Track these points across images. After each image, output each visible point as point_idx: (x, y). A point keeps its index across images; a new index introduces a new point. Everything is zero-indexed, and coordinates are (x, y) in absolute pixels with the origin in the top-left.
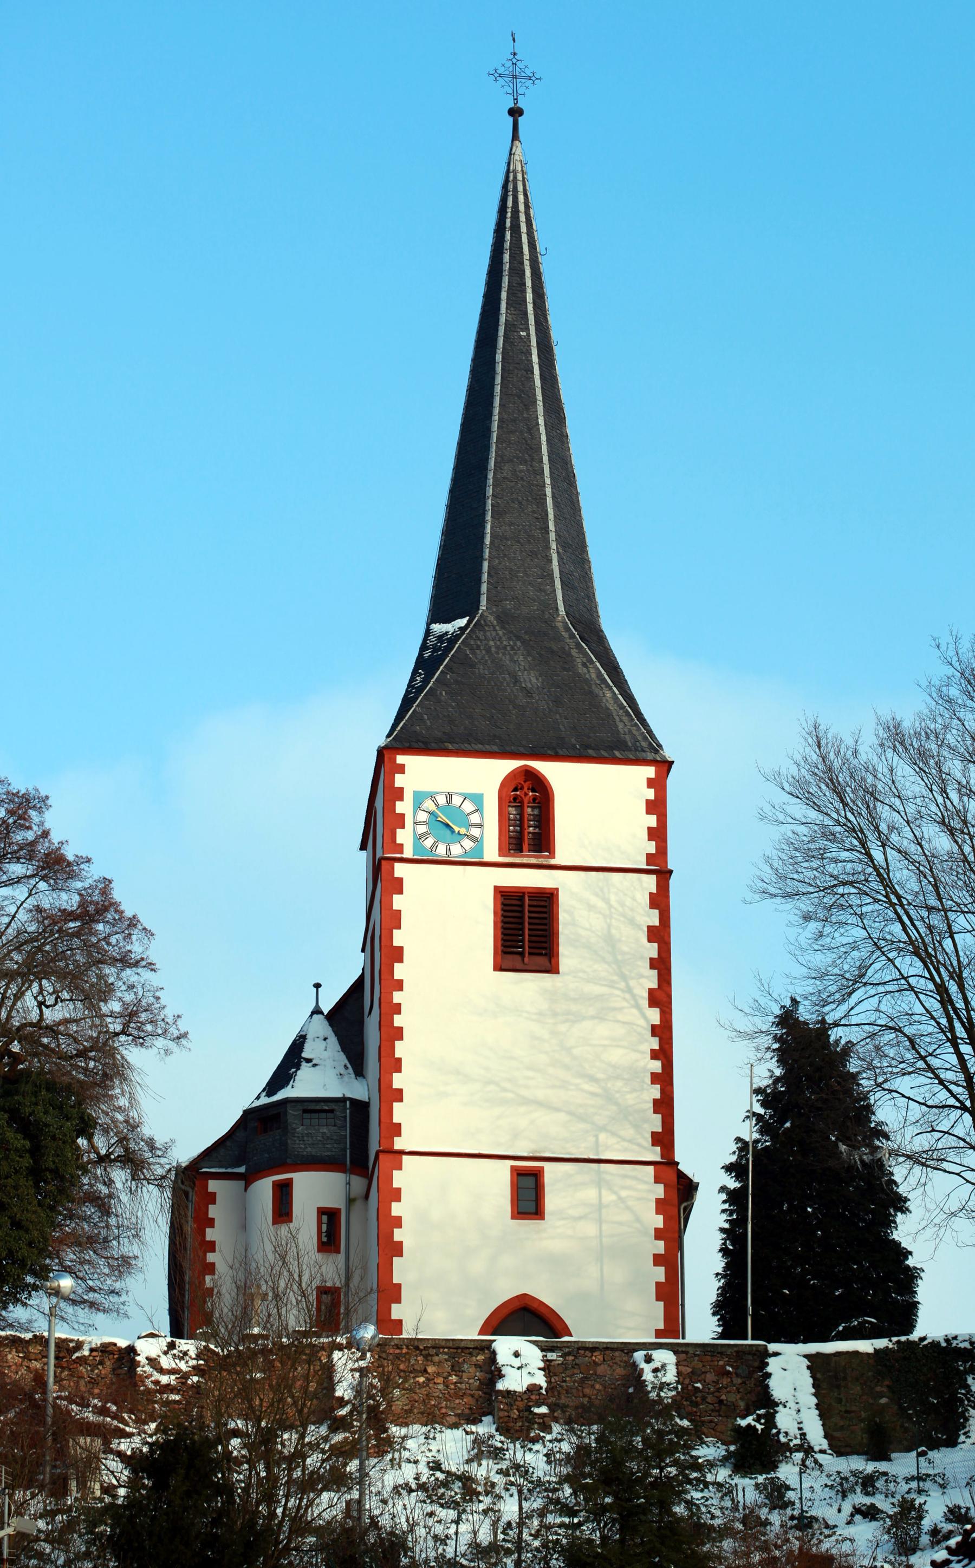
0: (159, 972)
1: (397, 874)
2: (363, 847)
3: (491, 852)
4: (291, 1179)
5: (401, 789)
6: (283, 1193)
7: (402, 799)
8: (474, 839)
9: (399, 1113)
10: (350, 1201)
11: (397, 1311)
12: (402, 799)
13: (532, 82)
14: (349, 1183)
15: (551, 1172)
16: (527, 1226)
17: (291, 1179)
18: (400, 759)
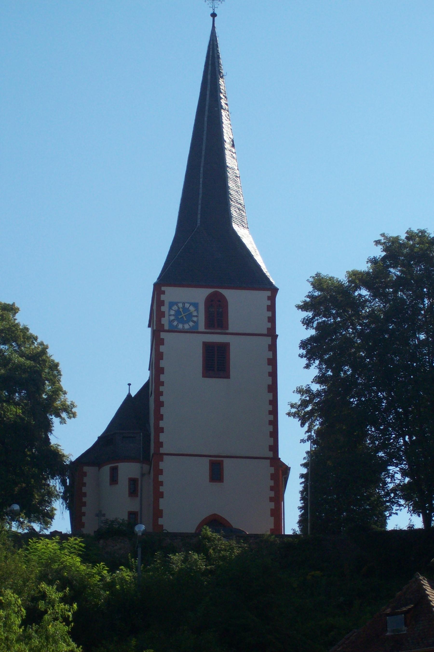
0: (299, 484)
1: (162, 337)
2: (149, 326)
3: (202, 327)
4: (117, 466)
5: (163, 301)
6: (114, 472)
7: (164, 305)
8: (194, 322)
9: (162, 437)
10: (143, 475)
11: (272, 470)
12: (164, 305)
13: (220, 2)
14: (142, 468)
15: (227, 463)
16: (216, 486)
17: (117, 466)
18: (163, 288)
